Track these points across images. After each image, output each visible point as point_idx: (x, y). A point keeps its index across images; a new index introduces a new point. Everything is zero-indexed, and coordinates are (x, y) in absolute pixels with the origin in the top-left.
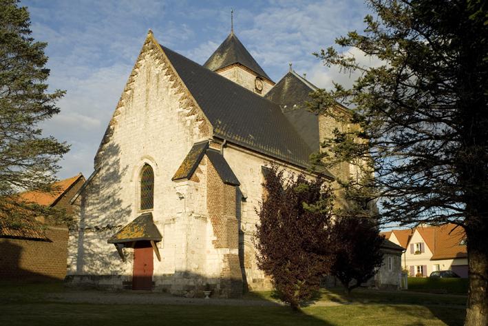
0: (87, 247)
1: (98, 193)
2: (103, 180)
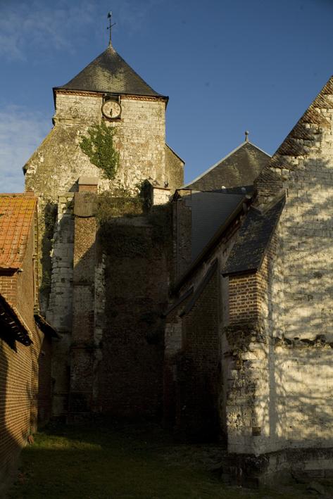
2: (293, 231)
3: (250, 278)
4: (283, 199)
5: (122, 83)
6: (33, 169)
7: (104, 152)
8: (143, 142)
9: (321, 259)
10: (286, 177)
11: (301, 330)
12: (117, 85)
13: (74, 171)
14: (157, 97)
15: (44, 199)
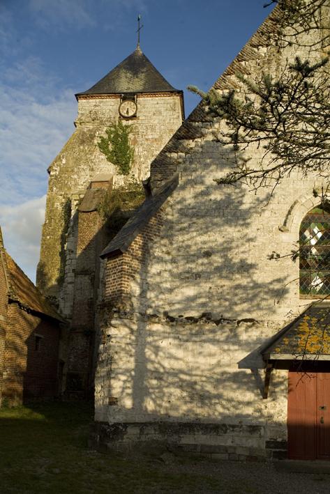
0: (153, 357)
1: (170, 237)
2: (183, 212)
3: (119, 259)
4: (176, 181)
5: (142, 82)
6: (56, 171)
7: (120, 149)
8: (156, 137)
9: (212, 238)
10: (180, 160)
11: (185, 309)
12: (137, 85)
13: (92, 170)
14: (172, 92)
15: (64, 197)
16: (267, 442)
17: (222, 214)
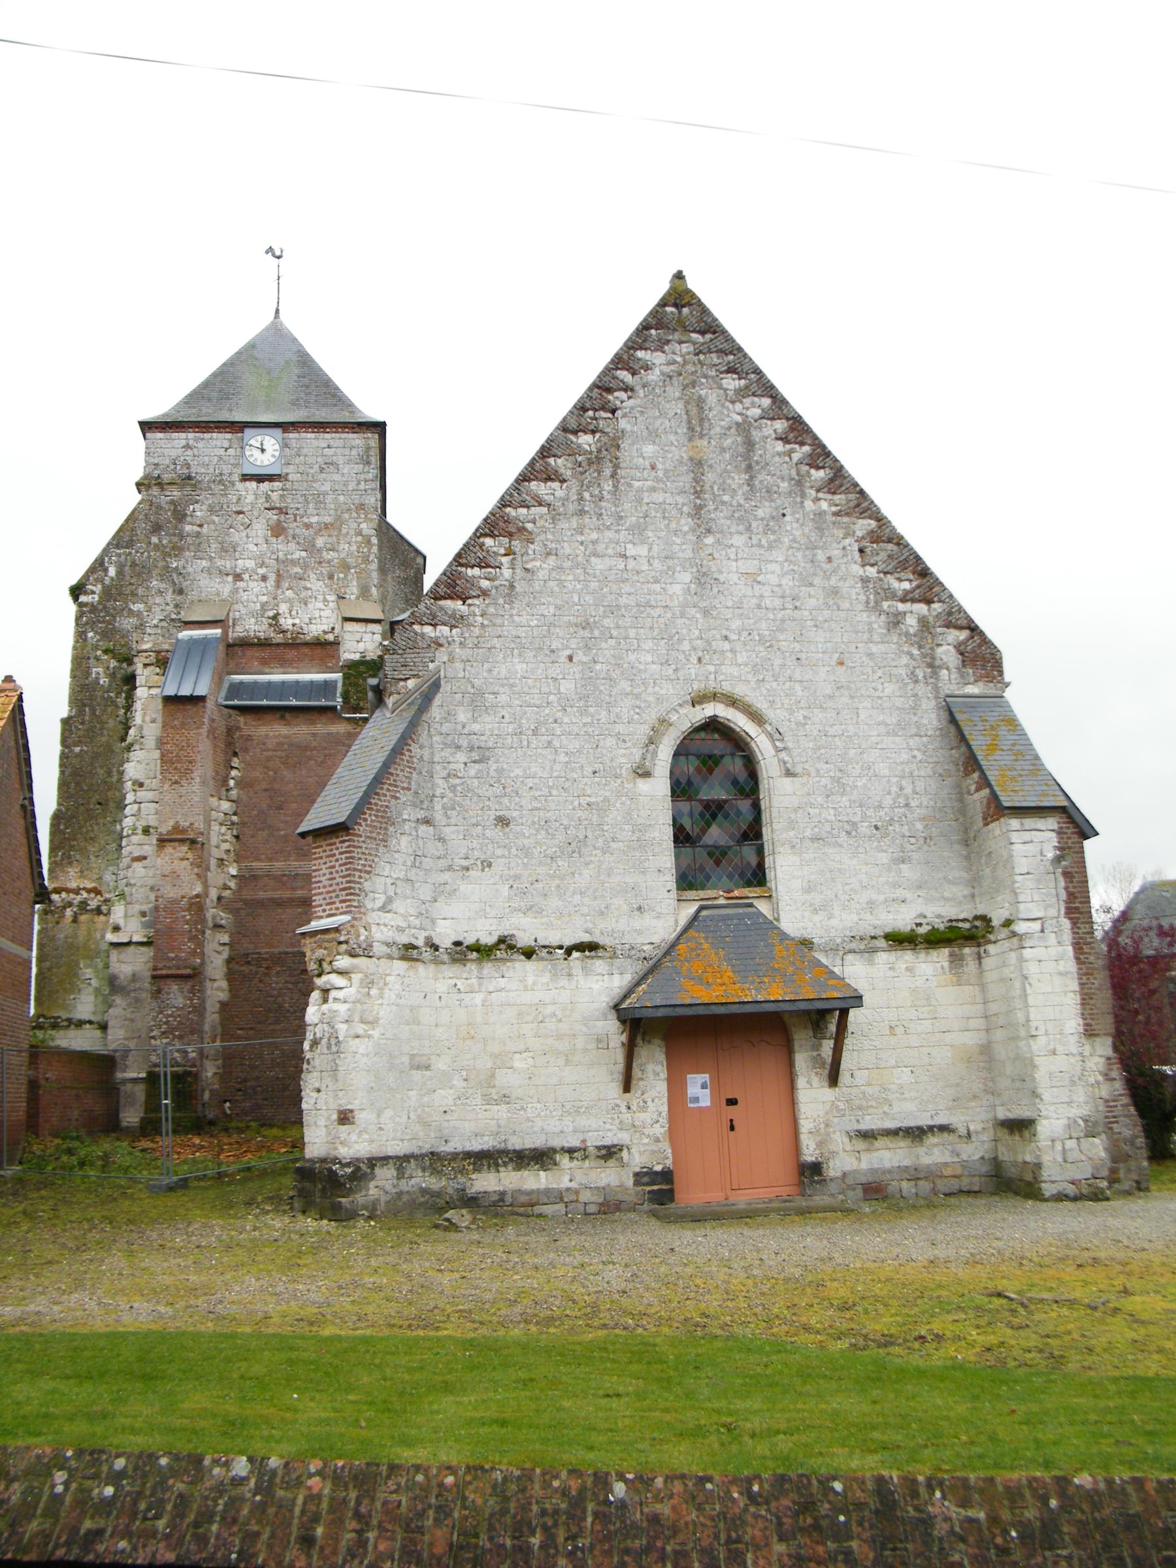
6: (93, 593)
8: (328, 519)
13: (181, 592)
16: (636, 1175)
17: (525, 743)
